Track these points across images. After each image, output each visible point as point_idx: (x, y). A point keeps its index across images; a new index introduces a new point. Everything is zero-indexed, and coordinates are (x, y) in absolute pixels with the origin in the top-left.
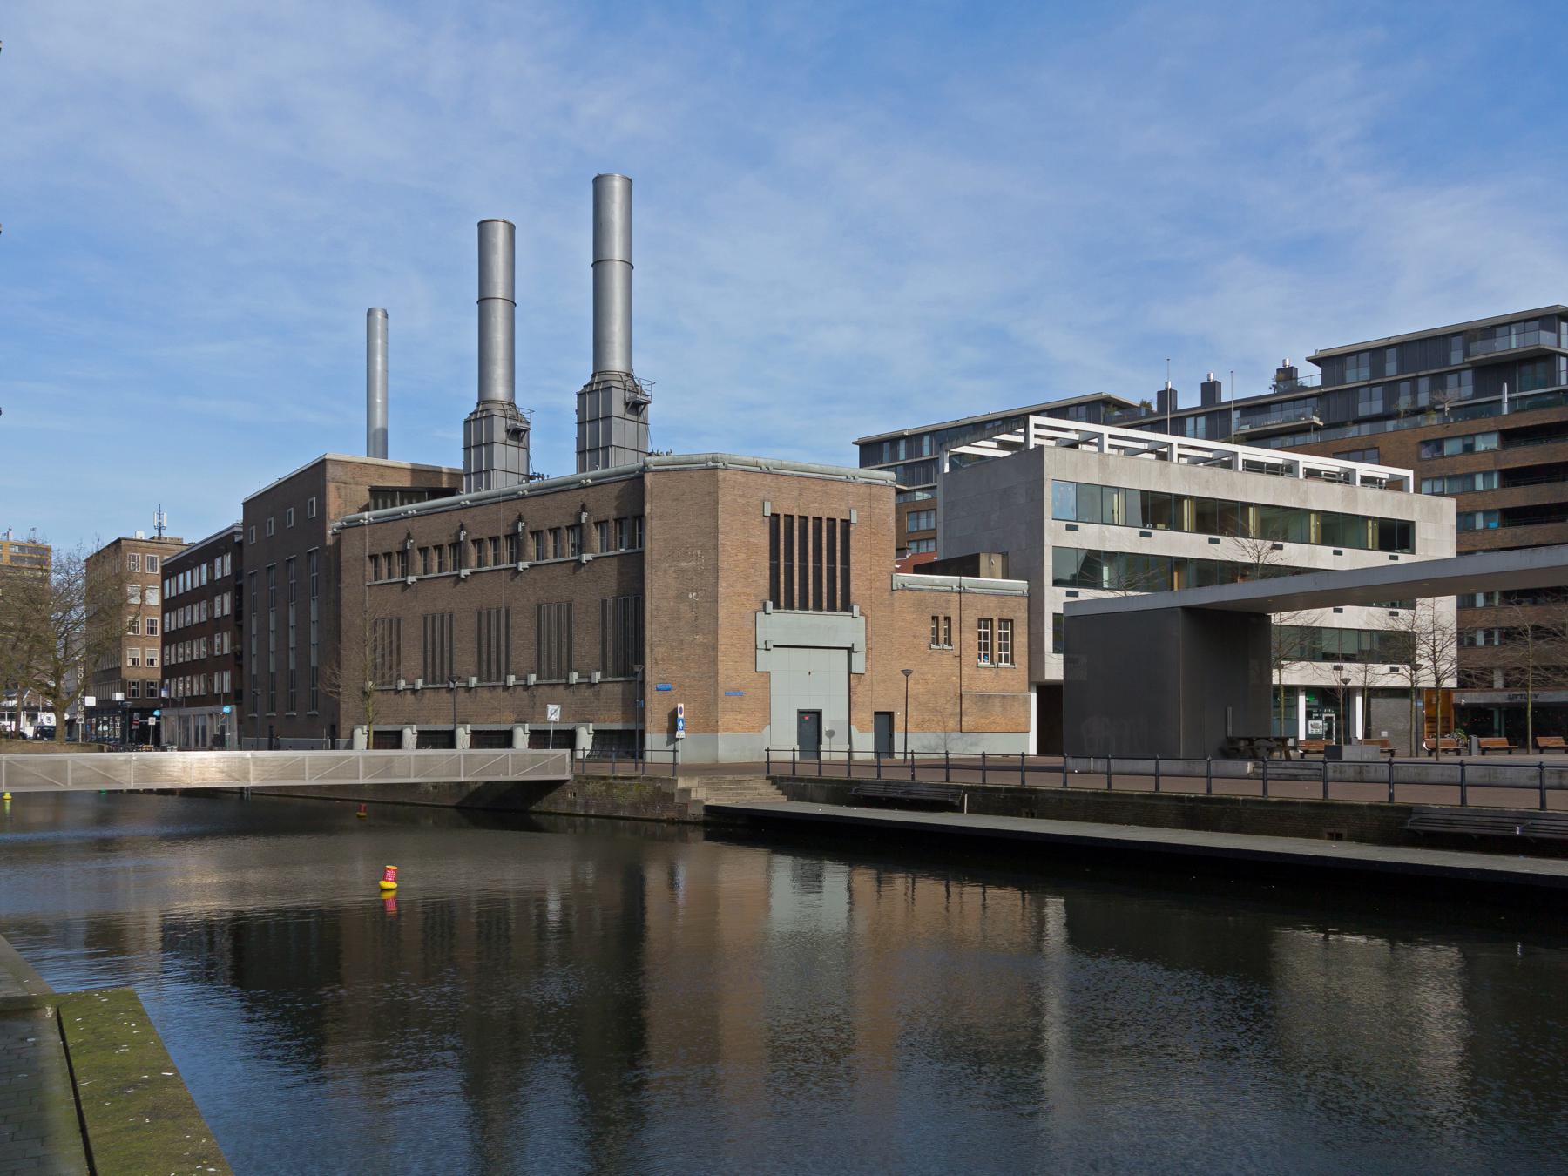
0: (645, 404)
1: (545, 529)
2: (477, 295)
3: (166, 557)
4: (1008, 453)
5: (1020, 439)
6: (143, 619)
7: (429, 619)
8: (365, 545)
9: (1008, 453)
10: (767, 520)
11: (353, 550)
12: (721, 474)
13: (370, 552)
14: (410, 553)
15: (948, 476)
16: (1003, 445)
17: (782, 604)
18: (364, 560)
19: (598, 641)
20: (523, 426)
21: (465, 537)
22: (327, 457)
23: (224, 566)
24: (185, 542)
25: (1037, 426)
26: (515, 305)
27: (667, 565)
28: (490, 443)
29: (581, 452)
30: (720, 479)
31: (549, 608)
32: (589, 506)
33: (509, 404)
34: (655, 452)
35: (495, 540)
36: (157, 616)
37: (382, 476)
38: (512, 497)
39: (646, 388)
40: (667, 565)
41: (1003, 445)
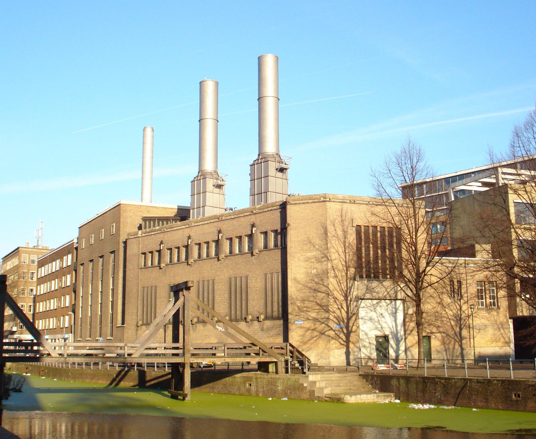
0: (286, 169)
1: (233, 237)
2: (258, 96)
3: (40, 256)
4: (487, 189)
5: (493, 181)
6: (28, 289)
7: (201, 283)
8: (139, 248)
9: (487, 189)
10: (354, 229)
11: (133, 249)
12: (328, 204)
13: (141, 251)
14: (255, 236)
15: (454, 202)
16: (485, 184)
17: (364, 276)
18: (139, 256)
19: (262, 297)
20: (284, 166)
21: (222, 237)
22: (121, 203)
23: (68, 260)
24: (50, 249)
25: (504, 173)
26: (218, 122)
27: (300, 255)
28: (205, 192)
29: (253, 195)
30: (328, 207)
31: (236, 279)
32: (256, 224)
33: (277, 154)
34: (292, 194)
35: (240, 238)
36: (35, 287)
37: (149, 212)
38: (219, 218)
39: (286, 161)
40: (300, 255)
41: (485, 184)
